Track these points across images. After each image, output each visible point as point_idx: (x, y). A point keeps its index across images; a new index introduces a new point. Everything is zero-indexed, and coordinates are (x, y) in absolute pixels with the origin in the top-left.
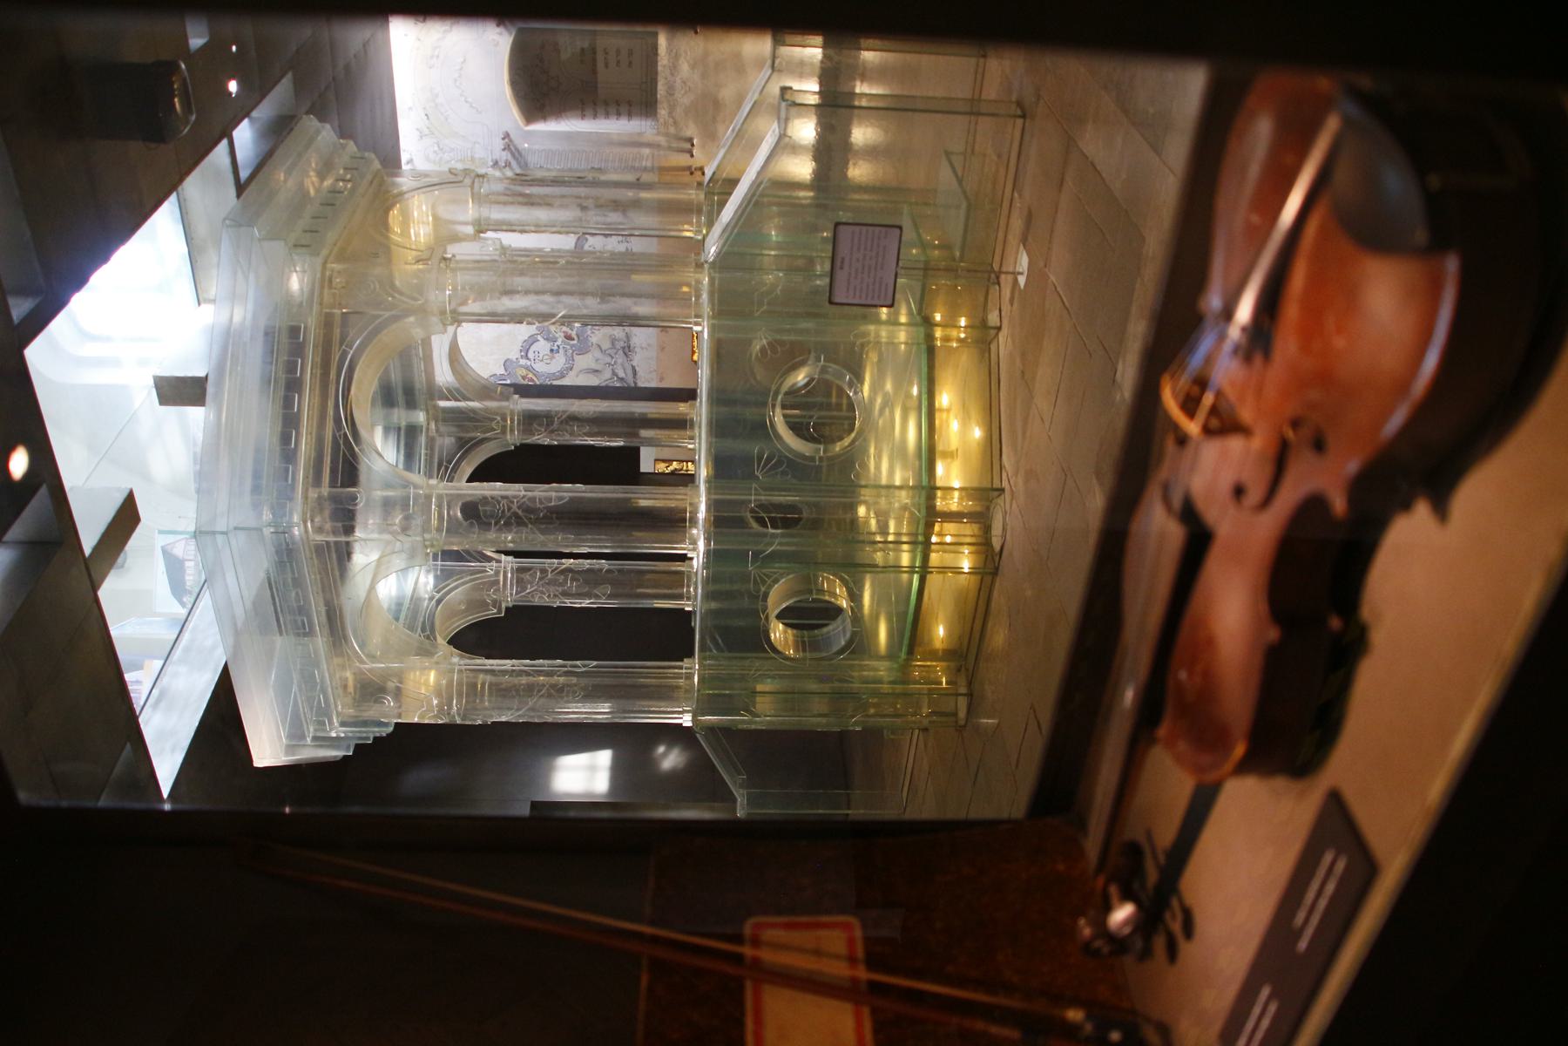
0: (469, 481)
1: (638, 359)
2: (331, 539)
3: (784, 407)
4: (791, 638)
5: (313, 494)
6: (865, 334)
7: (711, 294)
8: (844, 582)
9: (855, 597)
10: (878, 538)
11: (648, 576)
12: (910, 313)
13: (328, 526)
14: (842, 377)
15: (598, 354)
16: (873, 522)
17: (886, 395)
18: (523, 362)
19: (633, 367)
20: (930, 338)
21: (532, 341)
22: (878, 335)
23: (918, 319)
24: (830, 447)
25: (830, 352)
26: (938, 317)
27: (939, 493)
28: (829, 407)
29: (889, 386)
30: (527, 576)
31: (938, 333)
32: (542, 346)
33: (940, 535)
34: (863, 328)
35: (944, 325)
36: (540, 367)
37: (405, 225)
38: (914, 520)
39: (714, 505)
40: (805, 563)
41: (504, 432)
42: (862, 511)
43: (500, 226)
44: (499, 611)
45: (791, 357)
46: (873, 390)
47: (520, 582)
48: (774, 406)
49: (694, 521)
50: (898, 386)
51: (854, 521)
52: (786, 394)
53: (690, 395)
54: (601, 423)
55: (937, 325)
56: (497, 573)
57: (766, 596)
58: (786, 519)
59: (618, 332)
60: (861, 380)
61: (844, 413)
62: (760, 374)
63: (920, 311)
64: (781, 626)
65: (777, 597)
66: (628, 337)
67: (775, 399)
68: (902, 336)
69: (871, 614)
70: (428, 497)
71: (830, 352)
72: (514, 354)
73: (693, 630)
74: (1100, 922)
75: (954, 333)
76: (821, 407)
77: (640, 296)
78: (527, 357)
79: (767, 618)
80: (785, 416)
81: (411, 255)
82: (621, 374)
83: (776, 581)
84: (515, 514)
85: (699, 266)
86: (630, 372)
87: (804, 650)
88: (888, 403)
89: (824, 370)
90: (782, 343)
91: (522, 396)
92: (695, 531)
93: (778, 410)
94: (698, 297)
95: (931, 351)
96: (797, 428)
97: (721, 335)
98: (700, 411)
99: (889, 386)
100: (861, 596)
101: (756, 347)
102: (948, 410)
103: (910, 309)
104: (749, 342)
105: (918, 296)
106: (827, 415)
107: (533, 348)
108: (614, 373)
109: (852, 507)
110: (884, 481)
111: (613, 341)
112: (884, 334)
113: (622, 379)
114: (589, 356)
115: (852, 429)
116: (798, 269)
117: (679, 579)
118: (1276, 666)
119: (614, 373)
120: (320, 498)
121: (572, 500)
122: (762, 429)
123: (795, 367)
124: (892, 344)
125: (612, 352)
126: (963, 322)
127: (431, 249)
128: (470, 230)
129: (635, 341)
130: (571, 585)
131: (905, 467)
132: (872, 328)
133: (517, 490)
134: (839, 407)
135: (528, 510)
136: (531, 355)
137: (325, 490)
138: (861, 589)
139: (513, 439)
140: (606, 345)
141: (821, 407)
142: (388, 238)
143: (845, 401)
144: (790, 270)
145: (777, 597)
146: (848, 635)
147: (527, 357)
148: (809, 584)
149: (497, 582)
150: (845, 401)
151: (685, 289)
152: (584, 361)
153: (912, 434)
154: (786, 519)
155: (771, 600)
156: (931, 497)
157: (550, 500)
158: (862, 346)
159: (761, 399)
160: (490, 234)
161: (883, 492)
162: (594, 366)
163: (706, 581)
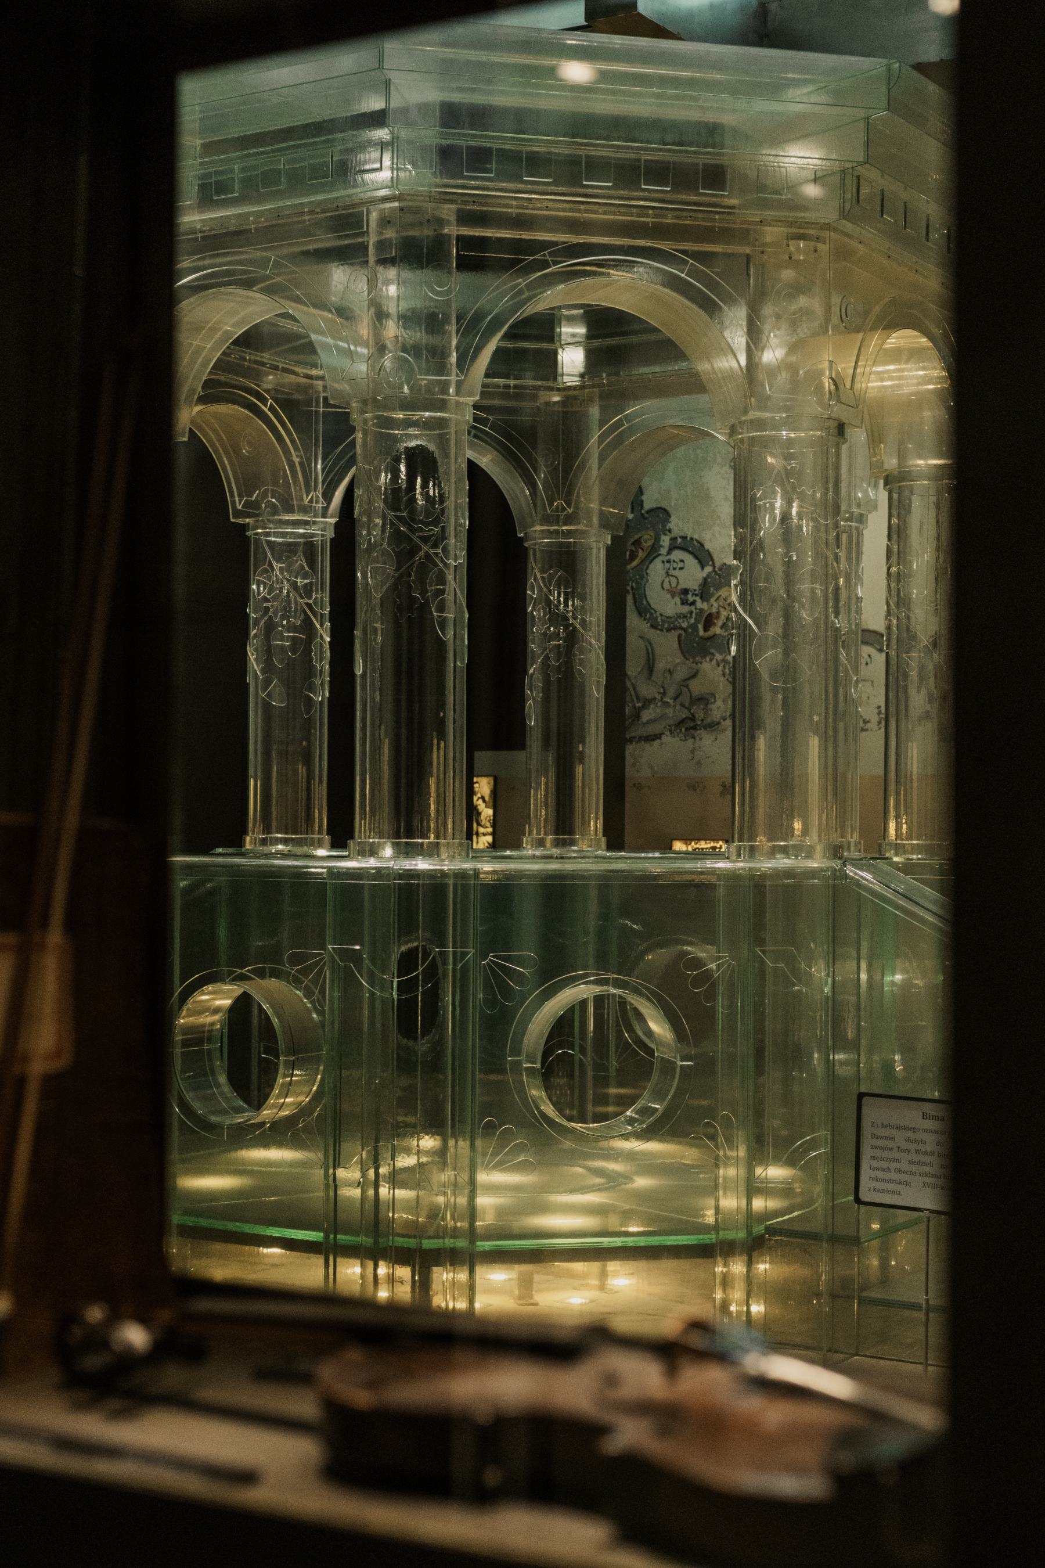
0: (471, 464)
1: (671, 746)
2: (372, 240)
3: (599, 1000)
4: (209, 1019)
5: (448, 211)
6: (730, 1141)
7: (789, 873)
8: (304, 1111)
9: (279, 1133)
10: (383, 1170)
11: (301, 769)
12: (767, 1215)
13: (390, 234)
14: (659, 1095)
15: (681, 674)
16: (406, 1161)
17: (628, 1178)
18: (665, 541)
19: (658, 736)
20: (727, 1249)
21: (703, 556)
22: (727, 1162)
23: (759, 1229)
24: (539, 1082)
25: (702, 1073)
26: (762, 1267)
27: (463, 1276)
28: (602, 1081)
29: (642, 1182)
30: (301, 561)
31: (738, 1268)
32: (692, 574)
33: (391, 1280)
34: (740, 1136)
35: (749, 1278)
36: (657, 569)
37: (895, 355)
38: (415, 1230)
39: (436, 883)
40: (347, 1044)
41: (546, 520)
42: (428, 1142)
43: (899, 508)
44: (238, 514)
45: (691, 1013)
46: (630, 1156)
47: (290, 549)
48: (599, 982)
49: (407, 851)
50: (643, 1196)
51: (403, 1130)
52: (623, 1003)
53: (615, 840)
54: (565, 685)
55: (750, 1264)
56: (304, 510)
57: (275, 974)
58: (417, 1013)
59: (720, 708)
60: (648, 1134)
61: (590, 1107)
62: (656, 958)
63: (772, 1231)
64: (227, 1002)
65: (276, 995)
66: (712, 726)
67: (617, 984)
68: (730, 1202)
69: (243, 1162)
70: (442, 405)
71: (702, 1073)
72: (678, 525)
73: (205, 851)
74: (116, 1316)
75: (737, 1294)
76: (601, 1067)
77: (784, 754)
78: (671, 549)
79: (243, 978)
80: (583, 1003)
81: (845, 367)
82: (646, 715)
83: (308, 994)
84: (414, 550)
85: (836, 852)
86: (650, 730)
87: (185, 1044)
88: (613, 1181)
89: (668, 1067)
90: (711, 995)
91: (609, 550)
92: (388, 851)
93: (597, 989)
94: (784, 850)
95: (705, 1252)
96: (563, 1027)
97: (721, 892)
98: (589, 856)
99: (642, 1182)
100: (280, 1144)
101: (701, 952)
102: (602, 1288)
103: (776, 1214)
104: (710, 938)
105: (797, 1227)
106: (593, 1073)
107: (690, 560)
108: (648, 702)
109: (434, 1124)
110: (482, 1177)
111: (704, 700)
112: (732, 1172)
113: (637, 715)
114: (679, 659)
115: (570, 1119)
116: (837, 1022)
117: (298, 826)
118: (440, 1425)
119: (648, 702)
120: (441, 222)
121: (441, 645)
122: (554, 971)
123: (672, 1019)
124: (713, 1188)
125: (685, 699)
126: (757, 1309)
127: (857, 403)
128: (891, 463)
129: (706, 739)
130: (283, 641)
131: (501, 1212)
132: (742, 1152)
133: (456, 556)
134: (602, 1100)
135: (423, 569)
136: (677, 555)
137: (452, 230)
138: (296, 1143)
139: (538, 535)
140: (697, 687)
141: (601, 1067)
142: (874, 328)
143: (611, 1109)
144: (835, 1009)
145: (276, 995)
146: (214, 1119)
147: (671, 549)
148: (303, 1051)
149: (290, 510)
150: (611, 1109)
151: (797, 825)
152: (667, 646)
153: (566, 1217)
154: (417, 1013)
155: (272, 983)
156: (453, 1257)
157: (441, 608)
158: (713, 1137)
159: (616, 957)
160: (883, 496)
161: (465, 1177)
162: (660, 665)
163: (298, 874)
